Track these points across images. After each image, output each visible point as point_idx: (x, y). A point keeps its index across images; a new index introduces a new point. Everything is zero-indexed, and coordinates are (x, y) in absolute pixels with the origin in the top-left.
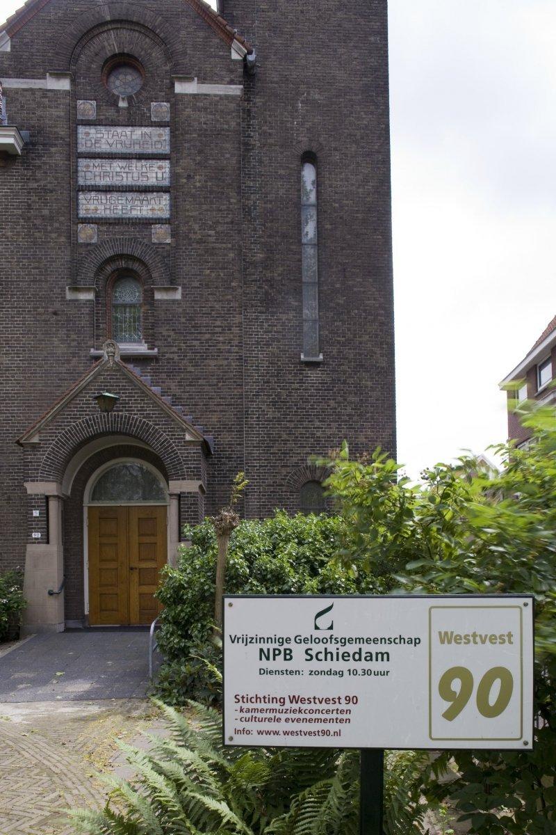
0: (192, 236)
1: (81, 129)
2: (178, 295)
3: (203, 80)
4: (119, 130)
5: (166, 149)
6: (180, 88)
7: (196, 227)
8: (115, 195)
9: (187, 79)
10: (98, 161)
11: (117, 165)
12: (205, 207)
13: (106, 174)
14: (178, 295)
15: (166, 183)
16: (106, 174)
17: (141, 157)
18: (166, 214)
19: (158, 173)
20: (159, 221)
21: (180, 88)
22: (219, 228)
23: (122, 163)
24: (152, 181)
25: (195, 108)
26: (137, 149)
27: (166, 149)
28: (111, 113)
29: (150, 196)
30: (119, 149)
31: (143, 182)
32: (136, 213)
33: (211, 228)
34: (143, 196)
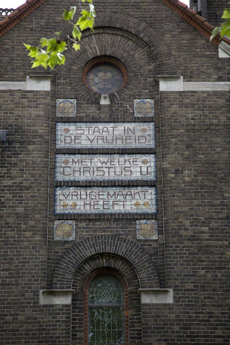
0: (183, 233)
1: (60, 127)
2: (169, 299)
3: (189, 77)
4: (101, 126)
5: (151, 144)
6: (164, 86)
7: (187, 223)
8: (96, 190)
9: (172, 77)
10: (77, 157)
11: (98, 160)
12: (195, 202)
13: (86, 169)
14: (169, 299)
15: (151, 177)
16: (86, 169)
17: (123, 152)
18: (152, 209)
19: (102, 252)
20: (145, 216)
21: (164, 86)
22: (213, 224)
23: (104, 158)
24: (136, 176)
25: (182, 105)
26: (119, 144)
27: (151, 144)
28: (92, 110)
29: (133, 190)
30: (100, 144)
31: (126, 177)
32: (118, 209)
33: (204, 224)
34: (126, 191)
